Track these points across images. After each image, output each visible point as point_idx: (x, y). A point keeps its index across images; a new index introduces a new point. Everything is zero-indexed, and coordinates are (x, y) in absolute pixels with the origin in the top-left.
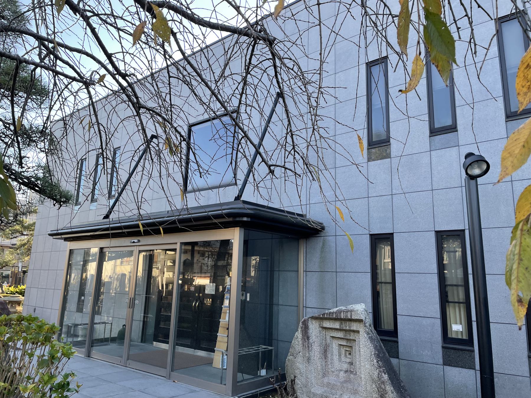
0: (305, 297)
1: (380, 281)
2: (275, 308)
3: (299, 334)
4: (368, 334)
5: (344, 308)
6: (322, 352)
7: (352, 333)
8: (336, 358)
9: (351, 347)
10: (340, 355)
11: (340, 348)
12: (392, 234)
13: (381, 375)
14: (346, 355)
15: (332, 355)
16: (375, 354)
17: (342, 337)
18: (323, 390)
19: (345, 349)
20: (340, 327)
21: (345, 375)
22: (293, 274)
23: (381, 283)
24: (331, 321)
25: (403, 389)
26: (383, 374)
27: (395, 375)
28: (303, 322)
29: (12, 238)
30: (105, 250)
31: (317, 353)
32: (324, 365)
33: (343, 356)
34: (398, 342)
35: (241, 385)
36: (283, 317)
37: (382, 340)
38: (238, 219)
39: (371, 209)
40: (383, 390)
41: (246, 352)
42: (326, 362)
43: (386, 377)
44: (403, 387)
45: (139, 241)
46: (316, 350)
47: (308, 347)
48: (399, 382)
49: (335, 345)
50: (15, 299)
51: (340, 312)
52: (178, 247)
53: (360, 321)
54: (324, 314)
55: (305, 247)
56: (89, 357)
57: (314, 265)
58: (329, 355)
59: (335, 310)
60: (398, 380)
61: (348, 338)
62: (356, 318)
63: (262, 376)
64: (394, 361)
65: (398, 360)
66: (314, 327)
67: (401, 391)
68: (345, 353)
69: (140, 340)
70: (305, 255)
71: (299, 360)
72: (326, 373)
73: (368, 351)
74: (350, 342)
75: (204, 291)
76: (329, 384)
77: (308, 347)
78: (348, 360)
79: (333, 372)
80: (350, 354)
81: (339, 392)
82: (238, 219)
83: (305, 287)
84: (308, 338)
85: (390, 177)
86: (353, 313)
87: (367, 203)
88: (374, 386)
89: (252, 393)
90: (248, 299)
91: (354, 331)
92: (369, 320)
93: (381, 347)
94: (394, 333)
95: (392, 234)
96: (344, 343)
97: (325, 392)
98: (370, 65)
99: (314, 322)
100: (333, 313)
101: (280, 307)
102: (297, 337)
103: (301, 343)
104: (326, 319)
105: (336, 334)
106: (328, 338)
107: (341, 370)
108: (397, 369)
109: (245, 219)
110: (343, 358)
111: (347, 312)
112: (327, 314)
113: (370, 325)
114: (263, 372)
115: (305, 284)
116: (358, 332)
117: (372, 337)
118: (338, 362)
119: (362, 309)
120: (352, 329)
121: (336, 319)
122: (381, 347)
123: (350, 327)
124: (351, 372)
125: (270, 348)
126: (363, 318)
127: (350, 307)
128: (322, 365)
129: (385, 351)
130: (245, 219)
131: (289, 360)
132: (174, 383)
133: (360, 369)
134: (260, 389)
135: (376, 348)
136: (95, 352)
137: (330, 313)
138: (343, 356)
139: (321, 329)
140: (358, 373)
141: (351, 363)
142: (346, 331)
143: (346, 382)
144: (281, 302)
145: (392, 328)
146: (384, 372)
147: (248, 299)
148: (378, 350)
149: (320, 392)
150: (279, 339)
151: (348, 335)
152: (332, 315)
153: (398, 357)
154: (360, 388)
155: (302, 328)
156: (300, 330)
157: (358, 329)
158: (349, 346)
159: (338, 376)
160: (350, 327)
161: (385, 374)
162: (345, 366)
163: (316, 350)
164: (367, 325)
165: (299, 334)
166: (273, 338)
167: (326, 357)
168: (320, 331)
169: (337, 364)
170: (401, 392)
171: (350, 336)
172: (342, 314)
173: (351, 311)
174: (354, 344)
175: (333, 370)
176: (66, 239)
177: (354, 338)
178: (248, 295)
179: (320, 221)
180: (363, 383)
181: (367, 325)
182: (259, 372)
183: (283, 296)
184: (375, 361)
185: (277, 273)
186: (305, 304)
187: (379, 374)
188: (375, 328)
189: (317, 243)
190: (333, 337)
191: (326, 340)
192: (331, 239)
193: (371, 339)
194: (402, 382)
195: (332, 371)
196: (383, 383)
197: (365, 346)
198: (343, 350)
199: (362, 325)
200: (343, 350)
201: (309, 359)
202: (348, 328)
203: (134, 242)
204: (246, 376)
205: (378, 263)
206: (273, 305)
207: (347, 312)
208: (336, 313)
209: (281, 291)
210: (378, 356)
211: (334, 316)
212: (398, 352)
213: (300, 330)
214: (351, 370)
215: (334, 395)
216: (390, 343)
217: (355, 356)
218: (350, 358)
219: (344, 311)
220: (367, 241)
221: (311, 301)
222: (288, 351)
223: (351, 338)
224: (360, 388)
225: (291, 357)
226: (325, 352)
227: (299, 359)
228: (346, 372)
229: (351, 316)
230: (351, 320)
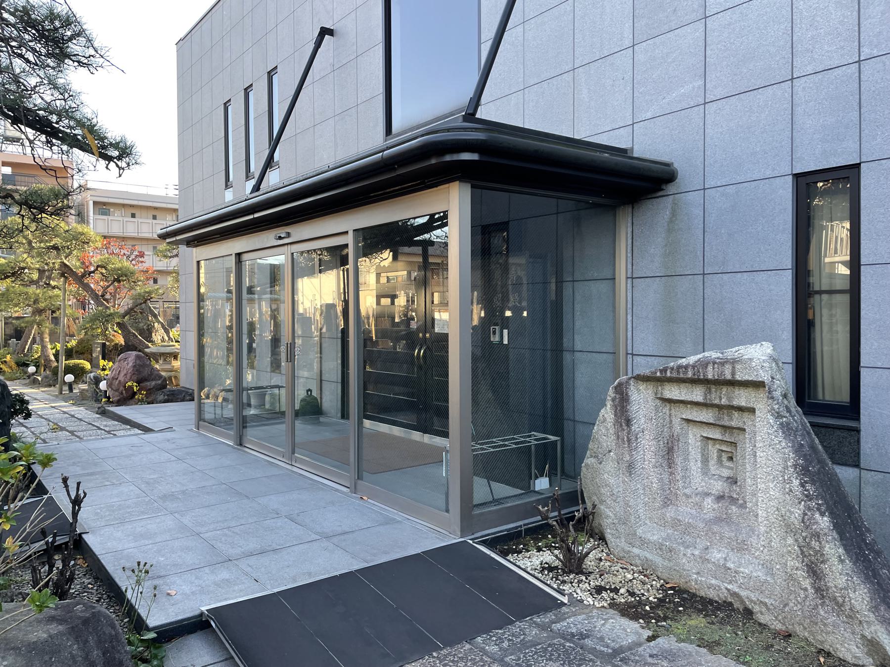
0: (629, 334)
1: (817, 288)
2: (567, 357)
3: (607, 413)
4: (779, 416)
5: (714, 355)
6: (661, 453)
7: (736, 414)
8: (695, 466)
9: (734, 444)
10: (705, 460)
11: (706, 445)
12: (857, 166)
13: (812, 518)
14: (720, 461)
15: (686, 459)
16: (795, 466)
17: (711, 421)
18: (664, 535)
19: (718, 446)
20: (705, 398)
21: (716, 506)
22: (604, 287)
23: (820, 292)
24: (682, 385)
25: (872, 550)
26: (817, 516)
27: (849, 517)
28: (616, 388)
29: (170, 257)
30: (245, 257)
31: (649, 455)
32: (666, 481)
33: (712, 463)
34: (858, 431)
35: (482, 514)
36: (584, 374)
37: (813, 425)
38: (448, 158)
39: (799, 110)
40: (816, 552)
41: (516, 444)
42: (671, 474)
43: (824, 522)
44: (871, 547)
45: (289, 235)
46: (647, 449)
47: (629, 440)
48: (862, 534)
49: (693, 438)
50: (168, 350)
51: (705, 364)
52: (349, 239)
53: (758, 385)
54: (664, 370)
55: (630, 224)
56: (241, 445)
57: (652, 259)
58: (679, 460)
59: (692, 359)
60: (857, 527)
61: (727, 424)
62: (746, 378)
63: (538, 493)
64: (845, 473)
65: (856, 470)
66: (642, 399)
67: (866, 557)
68: (719, 458)
69: (339, 415)
70: (630, 241)
71: (608, 468)
72: (673, 498)
73: (778, 459)
74: (731, 434)
75: (433, 327)
76: (676, 523)
77: (629, 440)
78: (726, 473)
79: (688, 497)
80: (731, 459)
81: (702, 543)
82: (448, 158)
83: (630, 311)
84: (628, 422)
85: (855, 14)
86: (738, 366)
87: (788, 95)
88: (790, 541)
89: (506, 530)
90: (506, 342)
91: (740, 409)
92: (783, 381)
93: (813, 447)
94: (852, 408)
95: (857, 166)
96: (716, 434)
97: (668, 537)
98: (805, 184)
99: (642, 386)
100: (686, 367)
101: (578, 355)
102: (605, 420)
103: (612, 431)
104: (671, 380)
105: (695, 413)
106: (676, 421)
107: (708, 494)
108: (854, 501)
109: (466, 156)
110: (713, 467)
111: (723, 364)
112: (672, 369)
113: (785, 396)
114: (542, 484)
115: (629, 306)
116: (752, 411)
117: (788, 424)
118: (699, 474)
119: (764, 356)
120: (735, 403)
121: (694, 381)
122: (813, 447)
123: (729, 399)
124: (733, 501)
125: (553, 438)
126: (764, 377)
127: (732, 352)
128: (661, 480)
129: (825, 456)
130: (466, 156)
131: (587, 465)
132: (361, 502)
133: (754, 495)
134: (526, 521)
135: (798, 450)
136: (251, 433)
137: (680, 367)
138: (712, 463)
139: (659, 403)
140: (749, 505)
141: (733, 481)
142: (720, 407)
143: (718, 520)
144: (578, 347)
145: (844, 397)
146: (818, 509)
147: (506, 342)
148: (805, 456)
149: (655, 538)
150: (577, 418)
151: (726, 418)
152: (686, 373)
153: (857, 465)
154: (754, 540)
155: (613, 400)
156: (609, 404)
157: (751, 405)
158: (728, 441)
159: (699, 506)
160: (729, 399)
161: (822, 514)
162: (718, 487)
163: (647, 449)
164: (777, 394)
165: (607, 413)
166: (566, 416)
167: (671, 463)
168: (657, 409)
169: (698, 481)
170: (866, 559)
171: (732, 419)
172: (710, 368)
173: (734, 362)
174: (741, 437)
175: (687, 491)
176: (190, 243)
177: (740, 425)
178: (505, 332)
179: (665, 159)
180: (762, 529)
181: (777, 394)
182: (532, 482)
183: (584, 333)
184: (796, 482)
185: (570, 285)
186: (630, 348)
187: (805, 514)
188: (800, 401)
189: (658, 211)
190: (688, 421)
191: (670, 428)
192: (694, 198)
193: (786, 428)
194: (868, 530)
195: (685, 494)
196: (817, 536)
197: (770, 448)
198: (713, 450)
199: (762, 394)
200: (713, 450)
201: (630, 467)
202: (724, 401)
203: (280, 238)
204: (502, 490)
205: (812, 265)
206: (562, 351)
207: (723, 364)
208: (693, 367)
209: (578, 324)
210: (804, 471)
211: (690, 374)
212: (859, 454)
213: (609, 404)
214: (732, 496)
215: (688, 547)
216: (838, 432)
217: (744, 465)
218: (732, 469)
219: (714, 363)
220: (785, 192)
221: (645, 344)
222: (586, 448)
223: (733, 424)
224: (754, 540)
225: (593, 460)
226: (669, 451)
227: (610, 465)
228: (720, 498)
229: (733, 374)
230: (733, 383)
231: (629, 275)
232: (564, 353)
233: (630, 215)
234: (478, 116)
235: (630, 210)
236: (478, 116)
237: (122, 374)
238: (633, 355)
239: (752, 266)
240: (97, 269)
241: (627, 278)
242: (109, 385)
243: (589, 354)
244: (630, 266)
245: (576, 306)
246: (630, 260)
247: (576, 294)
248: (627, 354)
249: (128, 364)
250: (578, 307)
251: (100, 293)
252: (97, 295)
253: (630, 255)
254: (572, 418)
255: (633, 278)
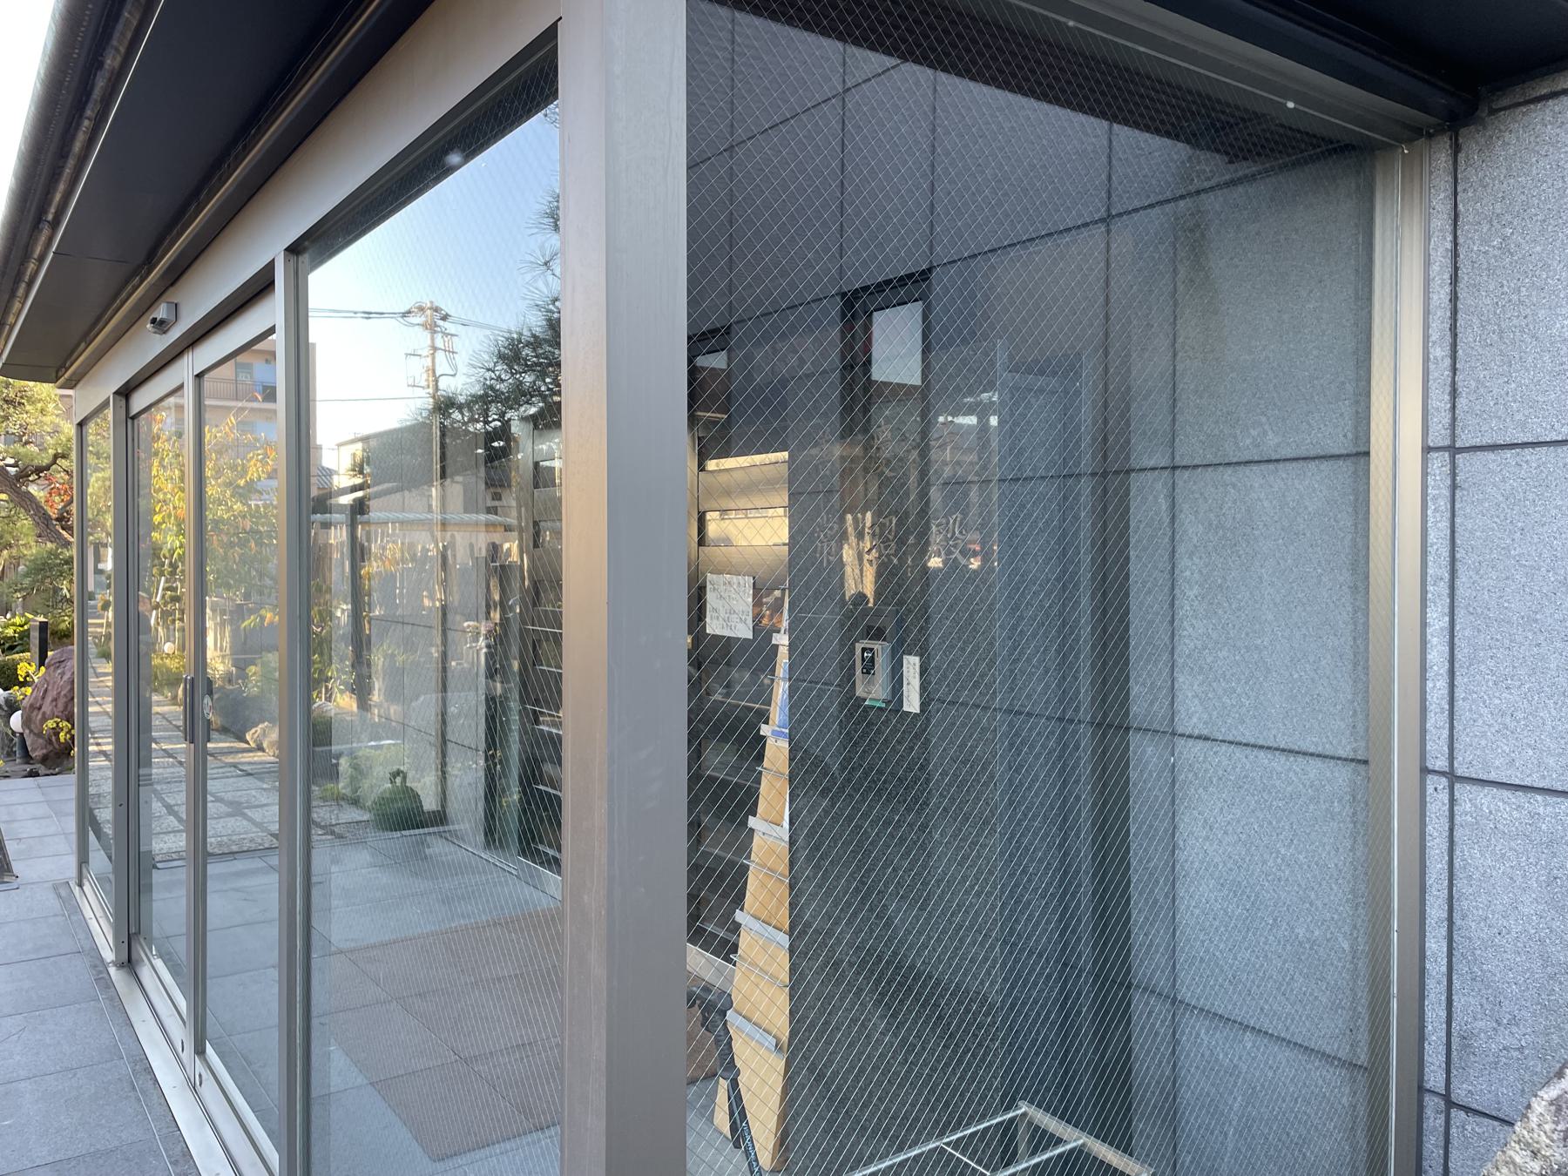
2: (1145, 754)
22: (1315, 488)
55: (1441, 221)
69: (481, 838)
70: (1441, 295)
90: (912, 704)
144: (1192, 717)
147: (912, 704)
150: (1185, 993)
178: (912, 664)
209: (1192, 632)
231: (1439, 436)
232: (1134, 739)
233: (1442, 183)
234: (916, 380)
235: (1442, 159)
236: (916, 380)
237: (49, 699)
238: (1453, 777)
239: (1523, 425)
240: (54, 462)
241: (1427, 450)
242: (26, 722)
243: (1239, 753)
244: (1440, 400)
245: (1183, 562)
246: (1441, 373)
247: (1186, 517)
248: (1425, 771)
249: (63, 674)
250: (1189, 568)
251: (53, 514)
252: (46, 518)
253: (1440, 352)
254: (1162, 983)
255: (1453, 450)
